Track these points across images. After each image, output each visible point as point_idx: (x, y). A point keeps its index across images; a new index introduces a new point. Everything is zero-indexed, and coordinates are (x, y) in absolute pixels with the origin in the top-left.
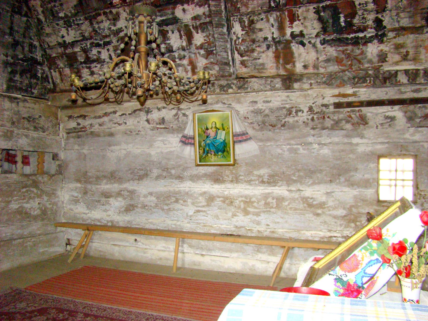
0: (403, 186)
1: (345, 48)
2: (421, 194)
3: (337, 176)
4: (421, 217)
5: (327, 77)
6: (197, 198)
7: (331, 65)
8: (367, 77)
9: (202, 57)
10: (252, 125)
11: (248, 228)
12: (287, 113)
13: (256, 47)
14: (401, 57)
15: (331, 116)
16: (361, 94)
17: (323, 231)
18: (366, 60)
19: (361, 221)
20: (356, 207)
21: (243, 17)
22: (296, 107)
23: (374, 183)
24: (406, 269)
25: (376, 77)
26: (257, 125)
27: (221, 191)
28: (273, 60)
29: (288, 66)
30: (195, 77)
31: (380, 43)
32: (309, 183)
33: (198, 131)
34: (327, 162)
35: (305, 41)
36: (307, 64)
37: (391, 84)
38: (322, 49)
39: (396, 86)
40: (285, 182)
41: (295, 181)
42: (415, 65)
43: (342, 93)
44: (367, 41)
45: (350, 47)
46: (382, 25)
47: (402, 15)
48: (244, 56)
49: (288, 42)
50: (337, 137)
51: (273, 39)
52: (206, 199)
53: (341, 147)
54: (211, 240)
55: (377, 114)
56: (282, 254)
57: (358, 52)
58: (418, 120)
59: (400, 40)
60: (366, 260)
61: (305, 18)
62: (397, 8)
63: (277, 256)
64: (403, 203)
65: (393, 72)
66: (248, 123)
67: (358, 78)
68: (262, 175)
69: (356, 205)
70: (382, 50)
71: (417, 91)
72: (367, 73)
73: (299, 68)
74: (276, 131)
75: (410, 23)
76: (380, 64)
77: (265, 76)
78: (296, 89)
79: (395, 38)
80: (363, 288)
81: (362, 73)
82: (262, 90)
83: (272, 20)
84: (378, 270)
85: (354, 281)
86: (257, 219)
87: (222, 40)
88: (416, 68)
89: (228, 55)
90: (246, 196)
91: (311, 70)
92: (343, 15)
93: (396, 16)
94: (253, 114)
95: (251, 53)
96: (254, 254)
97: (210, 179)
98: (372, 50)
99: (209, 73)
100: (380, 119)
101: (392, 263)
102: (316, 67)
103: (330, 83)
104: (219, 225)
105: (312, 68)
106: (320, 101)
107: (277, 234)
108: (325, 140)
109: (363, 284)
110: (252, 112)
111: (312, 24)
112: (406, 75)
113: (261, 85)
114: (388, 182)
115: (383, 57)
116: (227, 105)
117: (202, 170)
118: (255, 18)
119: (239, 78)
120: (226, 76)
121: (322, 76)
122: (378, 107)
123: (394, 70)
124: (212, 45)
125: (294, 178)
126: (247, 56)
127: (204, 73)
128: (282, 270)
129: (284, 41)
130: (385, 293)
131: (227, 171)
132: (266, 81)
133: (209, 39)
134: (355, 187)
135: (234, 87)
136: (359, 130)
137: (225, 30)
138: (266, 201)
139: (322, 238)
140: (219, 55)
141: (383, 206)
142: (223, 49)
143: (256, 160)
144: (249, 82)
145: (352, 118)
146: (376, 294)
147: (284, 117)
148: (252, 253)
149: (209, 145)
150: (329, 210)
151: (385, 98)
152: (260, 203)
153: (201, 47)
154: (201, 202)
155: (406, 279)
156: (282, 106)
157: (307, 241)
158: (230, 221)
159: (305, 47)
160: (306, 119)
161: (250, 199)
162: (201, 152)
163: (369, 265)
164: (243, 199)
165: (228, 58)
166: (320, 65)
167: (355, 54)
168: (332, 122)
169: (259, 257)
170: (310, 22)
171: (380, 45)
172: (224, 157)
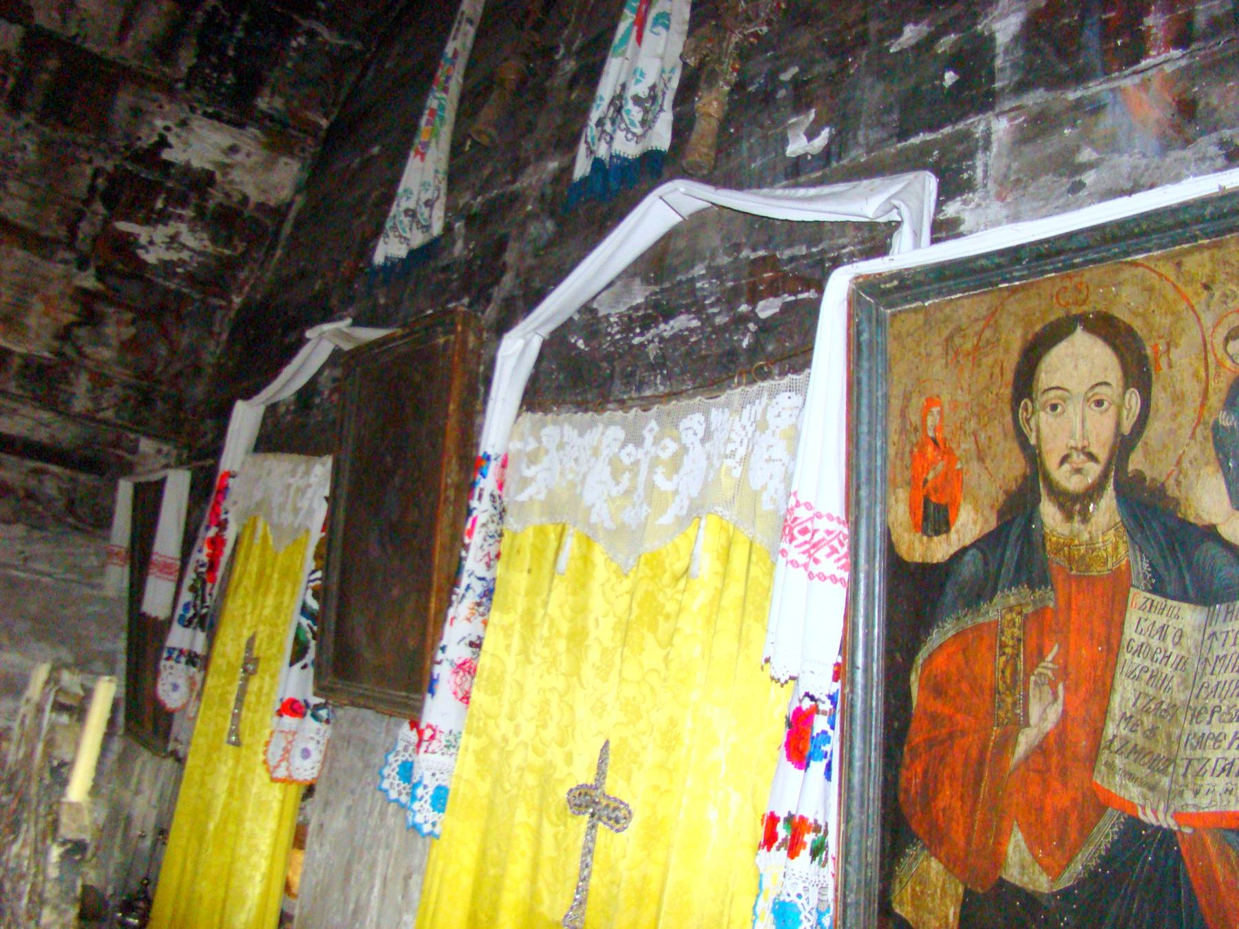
75: (28, 218)
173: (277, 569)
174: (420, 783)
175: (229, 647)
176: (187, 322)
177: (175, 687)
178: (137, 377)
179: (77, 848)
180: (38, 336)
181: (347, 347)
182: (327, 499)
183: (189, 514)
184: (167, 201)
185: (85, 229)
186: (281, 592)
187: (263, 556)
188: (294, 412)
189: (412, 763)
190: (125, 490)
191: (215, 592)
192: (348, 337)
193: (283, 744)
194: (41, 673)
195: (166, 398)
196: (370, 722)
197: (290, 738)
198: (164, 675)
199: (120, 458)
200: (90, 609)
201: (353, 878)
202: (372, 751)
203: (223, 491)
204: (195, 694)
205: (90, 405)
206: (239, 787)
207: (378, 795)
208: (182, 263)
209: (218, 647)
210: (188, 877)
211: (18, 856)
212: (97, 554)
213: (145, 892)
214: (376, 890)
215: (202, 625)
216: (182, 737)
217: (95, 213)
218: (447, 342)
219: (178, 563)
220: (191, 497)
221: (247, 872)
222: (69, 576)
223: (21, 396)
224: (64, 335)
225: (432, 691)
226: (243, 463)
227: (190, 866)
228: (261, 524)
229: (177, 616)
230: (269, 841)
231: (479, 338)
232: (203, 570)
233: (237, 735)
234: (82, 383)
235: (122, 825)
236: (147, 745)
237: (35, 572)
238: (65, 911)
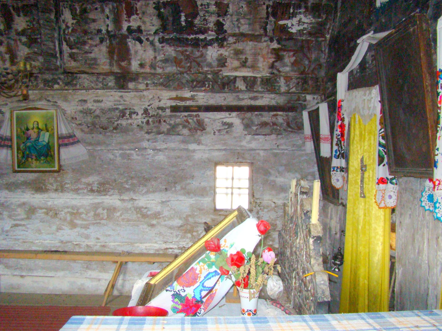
0: (240, 195)
1: (184, 49)
2: (256, 202)
3: (173, 184)
4: (258, 226)
5: (165, 78)
6: (14, 210)
7: (169, 66)
8: (206, 81)
9: (23, 45)
10: (81, 127)
11: (75, 243)
12: (120, 116)
13: (88, 39)
14: (241, 63)
15: (168, 120)
16: (200, 99)
17: (159, 242)
18: (205, 64)
19: (197, 231)
20: (192, 216)
21: (74, 4)
22: (130, 109)
23: (210, 191)
24: (244, 281)
25: (215, 81)
26: (86, 127)
27: (44, 202)
28: (106, 55)
29: (123, 64)
30: (14, 68)
31: (220, 47)
32: (143, 192)
33: (17, 131)
34: (162, 168)
35: (142, 38)
36: (143, 62)
37: (230, 90)
38: (161, 48)
39: (234, 93)
40: (117, 191)
41: (128, 190)
42: (253, 72)
43: (179, 96)
44: (208, 44)
45: (189, 49)
46: (223, 28)
47: (242, 21)
48: (73, 49)
49: (125, 37)
50: (174, 143)
51: (108, 31)
52: (25, 210)
53: (178, 153)
54: (32, 258)
55: (214, 120)
56: (115, 270)
57: (198, 54)
58: (255, 128)
59: (239, 46)
60: (204, 273)
61: (144, 13)
62: (239, 14)
63: (108, 273)
64: (240, 213)
65: (232, 78)
66: (76, 124)
67: (197, 81)
68: (91, 182)
70: (221, 55)
71: (255, 98)
72: (206, 77)
73: (135, 66)
74: (107, 134)
75: (249, 30)
76: (219, 69)
77: (98, 72)
78: (131, 89)
79: (235, 43)
80: (202, 302)
81: (200, 77)
82: (92, 88)
83: (107, 11)
84: (216, 283)
85: (193, 295)
86: (86, 232)
87: (48, 28)
88: (254, 75)
89: (55, 46)
90: (72, 207)
91: (147, 70)
92: (184, 14)
93: (237, 21)
94: (81, 115)
95: (82, 45)
96: (83, 272)
97: (30, 188)
98: (212, 53)
99: (31, 65)
100: (218, 126)
101: (230, 275)
102: (153, 66)
103: (168, 84)
104: (41, 241)
105: (148, 67)
106: (156, 104)
107: (109, 248)
108: (160, 145)
109: (201, 298)
110: (81, 112)
111: (151, 20)
112: (244, 81)
113: (92, 82)
114: (225, 191)
115: (222, 62)
116: (52, 103)
117: (21, 177)
118: (89, 7)
119: (66, 72)
120: (52, 70)
121: (159, 76)
122: (216, 113)
123: (233, 76)
124: (37, 32)
125: (127, 186)
126: (78, 48)
127: (25, 65)
128: (115, 287)
129: (120, 36)
130: (224, 305)
131: (50, 179)
132: (98, 78)
133: (34, 25)
134: (192, 195)
135: (61, 83)
136: (196, 136)
137: (53, 17)
138: (95, 212)
139: (157, 250)
140: (44, 45)
141: (220, 215)
142: (49, 38)
143: (84, 166)
144: (78, 77)
145: (189, 123)
146: (216, 307)
147: (116, 119)
148: (80, 270)
149: (29, 148)
150: (165, 221)
151: (223, 104)
152: (89, 215)
153: (23, 33)
154: (19, 215)
155: (244, 289)
156: (114, 107)
157: (142, 254)
158: (55, 236)
159: (143, 45)
160: (140, 122)
161: (78, 210)
162: (20, 156)
164: (70, 210)
165: (55, 49)
166: (157, 65)
167: (194, 56)
168: (168, 127)
169: (88, 275)
170: (149, 17)
171: (220, 49)
172: (47, 162)
173: (366, 131)
174: (437, 202)
175: (354, 163)
176: (313, 50)
177: (338, 180)
178: (300, 74)
179: (318, 239)
180: (264, 69)
181: (374, 42)
182: (380, 101)
183: (330, 119)
184: (294, 9)
185: (269, 28)
186: (370, 139)
187: (360, 128)
188: (360, 72)
189: (433, 194)
190: (305, 115)
191: (345, 144)
192: (373, 38)
193: (381, 195)
194: (294, 183)
195: (312, 78)
196: (413, 183)
197: (384, 192)
199: (301, 104)
200: (303, 159)
201: (416, 240)
202: (416, 192)
203: (340, 107)
204: (345, 182)
205: (287, 88)
206: (367, 213)
207: (421, 208)
208: (305, 29)
209: (350, 163)
210: (355, 246)
211: (299, 243)
212: (301, 139)
213: (341, 253)
214: (425, 244)
215: (343, 157)
216: (344, 197)
217: (271, 21)
218: (414, 30)
219: (330, 137)
220: (329, 112)
221: (376, 242)
222: (293, 149)
223: (263, 91)
224: (272, 66)
225: (436, 167)
226: (345, 95)
227: (354, 242)
228: (357, 116)
229: (333, 156)
230: (382, 230)
231: (427, 24)
232: (339, 137)
233: (364, 194)
234: (282, 81)
235: (328, 231)
237: (282, 150)
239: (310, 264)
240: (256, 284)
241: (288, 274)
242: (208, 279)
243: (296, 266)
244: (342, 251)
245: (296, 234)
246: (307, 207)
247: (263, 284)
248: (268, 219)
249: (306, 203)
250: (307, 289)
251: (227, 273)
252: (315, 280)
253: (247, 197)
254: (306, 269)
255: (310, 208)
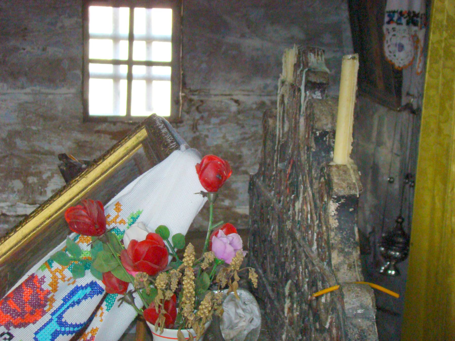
2: (191, 100)
4: (201, 170)
19: (39, 174)
23: (76, 70)
60: (64, 290)
69: (27, 130)
84: (94, 314)
101: (131, 293)
114: (109, 69)
134: (23, 79)
141: (98, 132)
163: (70, 302)
177: (401, 47)
179: (349, 204)
194: (290, 58)
198: (388, 37)
204: (419, 51)
210: (438, 214)
211: (302, 210)
213: (401, 229)
216: (414, 91)
227: (438, 205)
236: (383, 103)
238: (350, 253)
239: (329, 264)
240: (195, 318)
241: (273, 285)
242: (72, 305)
243: (293, 267)
244: (405, 224)
245: (294, 188)
246: (324, 122)
247: (213, 315)
248: (219, 142)
249: (321, 111)
250: (321, 325)
251: (122, 287)
252: (343, 307)
253: (168, 85)
254: (319, 276)
255: (330, 126)
